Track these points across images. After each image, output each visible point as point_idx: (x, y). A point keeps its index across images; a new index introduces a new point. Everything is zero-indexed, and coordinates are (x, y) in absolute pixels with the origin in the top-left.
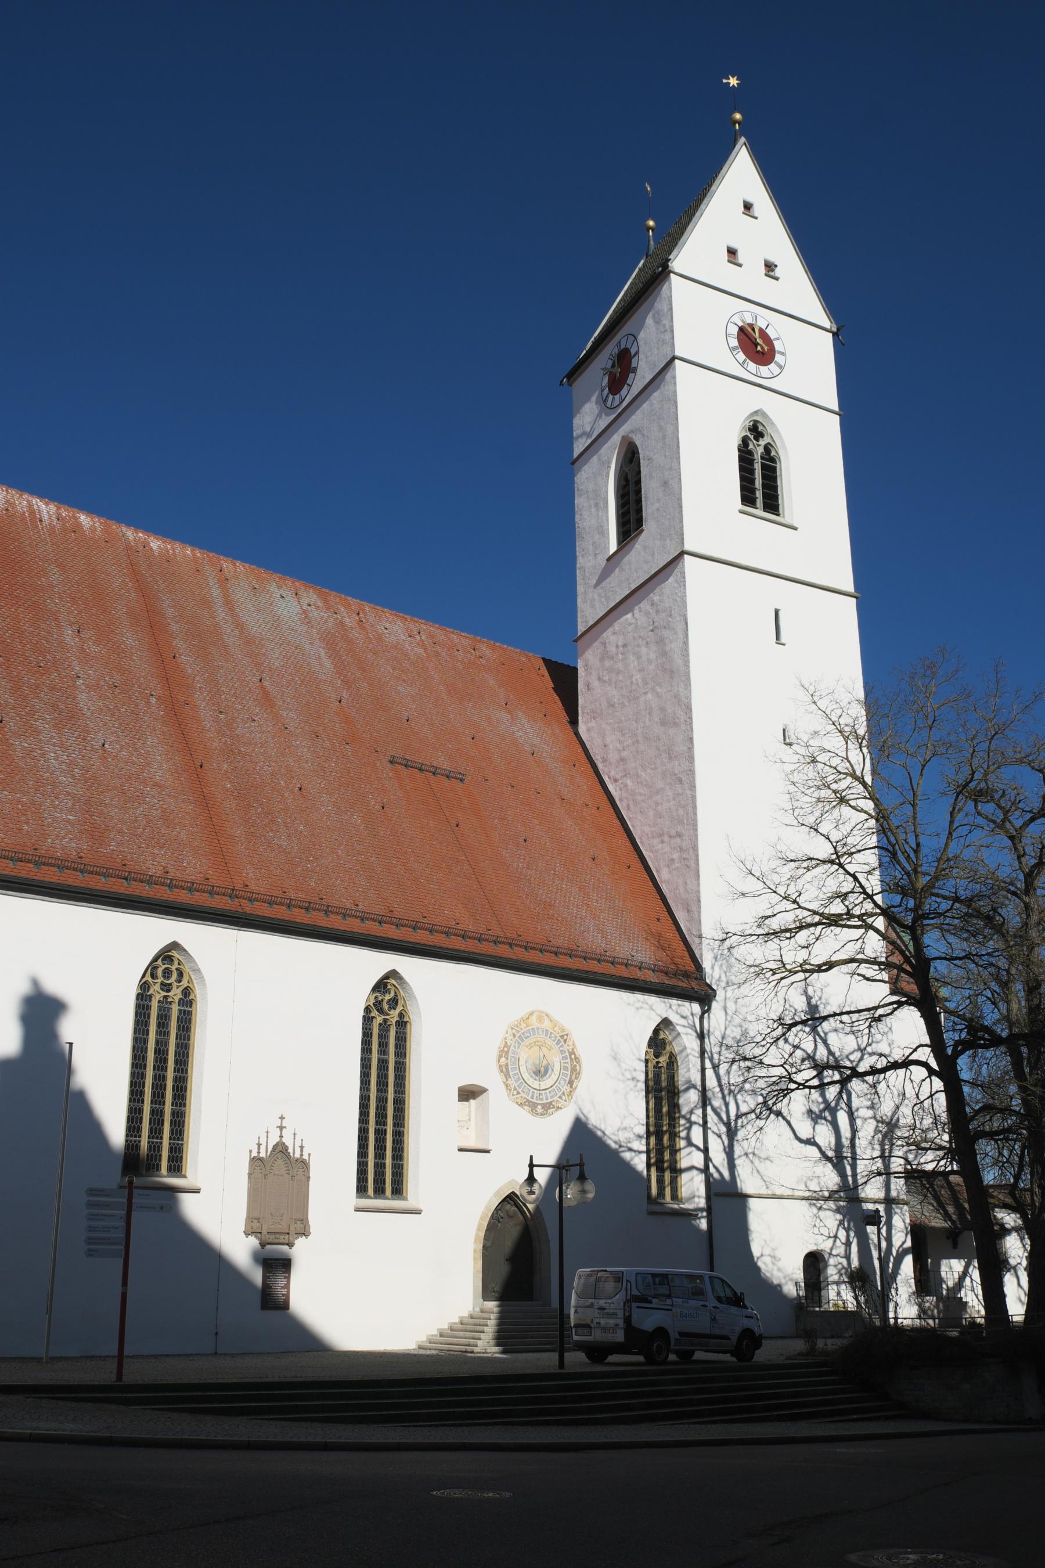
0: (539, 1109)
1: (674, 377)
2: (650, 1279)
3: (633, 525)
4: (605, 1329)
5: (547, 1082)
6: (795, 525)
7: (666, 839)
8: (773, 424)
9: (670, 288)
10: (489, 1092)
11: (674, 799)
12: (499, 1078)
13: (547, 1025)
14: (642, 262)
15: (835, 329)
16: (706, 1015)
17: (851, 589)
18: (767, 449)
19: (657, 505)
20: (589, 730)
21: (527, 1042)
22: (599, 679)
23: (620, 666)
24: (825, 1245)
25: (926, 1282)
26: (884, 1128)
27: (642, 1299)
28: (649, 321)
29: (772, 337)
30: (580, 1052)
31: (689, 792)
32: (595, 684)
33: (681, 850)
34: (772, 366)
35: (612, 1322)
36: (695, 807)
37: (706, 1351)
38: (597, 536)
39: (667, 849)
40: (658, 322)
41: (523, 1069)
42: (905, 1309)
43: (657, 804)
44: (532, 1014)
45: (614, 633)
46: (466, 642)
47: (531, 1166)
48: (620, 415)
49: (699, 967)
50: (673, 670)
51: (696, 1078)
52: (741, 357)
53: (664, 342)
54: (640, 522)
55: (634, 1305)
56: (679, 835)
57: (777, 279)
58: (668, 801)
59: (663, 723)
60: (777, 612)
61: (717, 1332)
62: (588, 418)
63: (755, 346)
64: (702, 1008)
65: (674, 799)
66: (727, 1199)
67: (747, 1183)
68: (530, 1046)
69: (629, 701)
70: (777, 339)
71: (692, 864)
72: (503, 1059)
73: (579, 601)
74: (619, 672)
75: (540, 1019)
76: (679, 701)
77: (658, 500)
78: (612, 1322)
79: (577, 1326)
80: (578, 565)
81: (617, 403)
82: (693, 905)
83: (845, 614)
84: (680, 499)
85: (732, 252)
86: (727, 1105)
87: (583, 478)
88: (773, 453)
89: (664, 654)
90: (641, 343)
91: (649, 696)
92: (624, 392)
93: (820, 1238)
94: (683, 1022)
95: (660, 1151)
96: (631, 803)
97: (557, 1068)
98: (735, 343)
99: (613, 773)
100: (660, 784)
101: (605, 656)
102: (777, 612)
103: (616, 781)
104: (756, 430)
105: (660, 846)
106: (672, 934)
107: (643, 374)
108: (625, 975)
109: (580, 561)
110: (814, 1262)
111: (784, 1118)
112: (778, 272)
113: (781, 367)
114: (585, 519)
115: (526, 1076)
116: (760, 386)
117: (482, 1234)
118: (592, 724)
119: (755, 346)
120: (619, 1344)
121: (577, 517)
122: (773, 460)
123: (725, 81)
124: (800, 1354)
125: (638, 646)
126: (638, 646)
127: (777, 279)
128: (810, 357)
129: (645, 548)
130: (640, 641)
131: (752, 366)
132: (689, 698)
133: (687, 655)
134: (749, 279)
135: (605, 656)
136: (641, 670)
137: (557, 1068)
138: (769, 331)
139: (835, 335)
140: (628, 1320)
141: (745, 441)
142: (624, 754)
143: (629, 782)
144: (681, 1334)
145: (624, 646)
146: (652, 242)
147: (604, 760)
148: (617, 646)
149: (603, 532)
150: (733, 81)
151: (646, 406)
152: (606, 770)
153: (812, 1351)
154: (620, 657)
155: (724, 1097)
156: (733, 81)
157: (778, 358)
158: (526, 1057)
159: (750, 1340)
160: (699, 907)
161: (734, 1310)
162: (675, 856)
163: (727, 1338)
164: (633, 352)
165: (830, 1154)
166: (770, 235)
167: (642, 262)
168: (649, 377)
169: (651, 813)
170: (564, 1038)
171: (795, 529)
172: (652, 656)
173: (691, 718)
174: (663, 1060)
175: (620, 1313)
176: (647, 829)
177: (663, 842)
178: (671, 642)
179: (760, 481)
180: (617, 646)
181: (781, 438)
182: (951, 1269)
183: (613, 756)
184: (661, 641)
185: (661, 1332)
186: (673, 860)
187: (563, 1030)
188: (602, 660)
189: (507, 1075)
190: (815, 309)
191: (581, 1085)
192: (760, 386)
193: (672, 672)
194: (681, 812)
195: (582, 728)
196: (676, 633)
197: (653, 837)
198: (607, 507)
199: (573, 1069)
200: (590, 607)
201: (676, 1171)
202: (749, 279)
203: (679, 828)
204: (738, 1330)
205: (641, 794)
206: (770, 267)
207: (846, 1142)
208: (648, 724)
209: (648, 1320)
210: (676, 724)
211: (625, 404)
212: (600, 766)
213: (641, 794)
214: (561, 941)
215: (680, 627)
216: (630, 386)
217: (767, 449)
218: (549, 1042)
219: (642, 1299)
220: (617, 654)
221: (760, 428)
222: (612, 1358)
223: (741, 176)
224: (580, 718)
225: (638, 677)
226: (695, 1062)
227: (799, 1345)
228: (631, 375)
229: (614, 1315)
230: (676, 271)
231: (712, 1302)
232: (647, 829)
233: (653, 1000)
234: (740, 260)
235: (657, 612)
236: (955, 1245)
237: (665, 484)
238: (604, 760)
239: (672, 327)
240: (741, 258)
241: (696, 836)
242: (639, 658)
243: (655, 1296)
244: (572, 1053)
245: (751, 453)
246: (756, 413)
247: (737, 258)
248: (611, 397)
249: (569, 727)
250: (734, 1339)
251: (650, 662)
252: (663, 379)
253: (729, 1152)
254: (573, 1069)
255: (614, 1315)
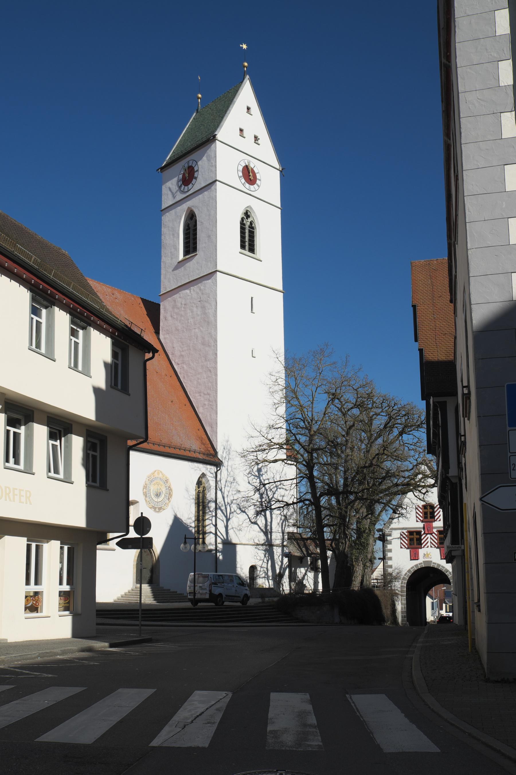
0: (157, 510)
1: (216, 189)
2: (217, 577)
3: (191, 249)
4: (201, 594)
5: (160, 499)
6: (261, 259)
7: (202, 394)
8: (254, 212)
9: (216, 147)
10: (140, 503)
11: (207, 378)
12: (143, 497)
13: (161, 476)
14: (195, 114)
15: (281, 169)
16: (219, 472)
17: (281, 288)
18: (251, 223)
19: (204, 245)
20: (165, 338)
21: (153, 483)
22: (171, 316)
23: (182, 313)
24: (258, 563)
25: (292, 577)
26: (283, 518)
27: (215, 584)
28: (205, 158)
29: (256, 172)
30: (172, 487)
31: (214, 377)
32: (169, 318)
33: (209, 401)
34: (255, 186)
35: (204, 591)
36: (216, 384)
37: (229, 602)
38: (173, 250)
39: (202, 399)
40: (209, 160)
41: (152, 494)
42: (286, 587)
43: (198, 379)
44: (155, 471)
45: (180, 297)
46: (109, 290)
47: (185, 538)
48: (187, 196)
49: (215, 450)
50: (209, 321)
51: (213, 496)
52: (243, 181)
53: (211, 171)
54: (195, 249)
55: (213, 586)
56: (209, 394)
57: (259, 144)
58: (204, 379)
59: (203, 344)
60: (252, 298)
61: (237, 595)
62: (170, 189)
63: (249, 175)
64: (217, 469)
65: (207, 378)
66: (230, 547)
67: (234, 540)
68: (154, 485)
69: (186, 330)
70: (258, 173)
71: (215, 408)
72: (145, 490)
73: (162, 277)
74: (182, 316)
75: (158, 473)
76: (211, 336)
77: (205, 243)
78: (204, 591)
79: (189, 593)
80: (162, 260)
81: (186, 190)
82: (214, 425)
83: (277, 301)
84: (216, 246)
85: (241, 130)
86: (226, 509)
87: (167, 218)
88: (253, 225)
89: (205, 313)
90: (200, 167)
91: (197, 330)
92: (190, 186)
93: (257, 561)
94: (211, 475)
95: (198, 527)
96: (185, 376)
97: (164, 492)
98: (241, 174)
99: (177, 361)
100: (200, 370)
101: (174, 307)
102: (252, 298)
103: (178, 364)
104: (247, 214)
105: (199, 397)
106: (204, 436)
107: (199, 183)
108: (189, 455)
109: (163, 259)
110: (253, 569)
111: (246, 514)
112: (259, 142)
113: (259, 186)
114: (166, 238)
115: (153, 496)
116: (250, 195)
117: (136, 558)
118: (167, 336)
119: (249, 175)
120: (207, 599)
121: (163, 237)
122: (253, 228)
123: (241, 46)
124: (260, 603)
125: (192, 306)
126: (192, 306)
127: (259, 144)
128: (270, 181)
129: (198, 263)
130: (193, 305)
131: (247, 185)
132: (216, 335)
133: (216, 317)
134: (247, 144)
135: (174, 307)
136: (193, 318)
137: (164, 492)
138: (254, 169)
139: (281, 172)
140: (210, 591)
141: (242, 219)
142: (183, 353)
143: (185, 366)
144: (226, 596)
145: (185, 304)
146: (200, 105)
147: (173, 354)
148: (181, 304)
149: (177, 249)
150: (245, 47)
151: (200, 196)
152: (173, 358)
153: (263, 602)
154: (183, 309)
155: (225, 506)
156: (245, 47)
157: (258, 182)
158: (153, 489)
159: (247, 597)
160: (217, 426)
161: (242, 587)
162: (206, 403)
163: (239, 597)
164: (196, 169)
165: (263, 528)
166: (256, 124)
167: (195, 114)
168: (203, 185)
169: (195, 382)
170: (167, 481)
171: (261, 261)
172: (199, 313)
173: (217, 345)
174: (201, 489)
175: (208, 589)
176: (193, 389)
177: (200, 396)
178: (209, 309)
179: (248, 240)
180: (181, 304)
181: (257, 219)
182: (301, 572)
183: (177, 353)
184: (203, 307)
185: (220, 595)
186: (205, 404)
187: (166, 478)
188: (173, 308)
189: (146, 496)
190: (274, 161)
191: (173, 499)
192: (250, 195)
193: (208, 323)
194: (210, 384)
195: (161, 337)
196: (211, 306)
197: (196, 393)
198: (179, 237)
199: (170, 494)
200: (168, 281)
201: (204, 533)
202: (247, 144)
203: (209, 391)
204: (243, 594)
205: (191, 373)
206: (256, 138)
207: (269, 524)
208: (195, 342)
209: (217, 591)
210: (209, 346)
211: (190, 192)
212: (170, 356)
213: (191, 373)
214: (165, 441)
215: (213, 303)
216: (194, 185)
217: (251, 223)
218: (161, 483)
219: (215, 584)
220: (181, 307)
221: (249, 213)
222: (199, 604)
223: (246, 95)
224: (160, 332)
225: (191, 320)
226: (213, 491)
227: (260, 600)
228: (194, 180)
229: (205, 589)
230: (219, 139)
231: (236, 585)
232: (193, 389)
233: (201, 466)
234: (245, 136)
235: (202, 294)
236: (301, 562)
237: (209, 237)
238: (173, 354)
239: (216, 165)
240: (245, 133)
241: (217, 396)
242: (192, 312)
243: (219, 583)
244: (169, 487)
245: (244, 225)
246: (248, 207)
247: (244, 132)
248: (183, 186)
249: (155, 335)
250: (242, 597)
251: (198, 315)
252: (210, 188)
253: (227, 527)
254: (170, 494)
255: (205, 589)
